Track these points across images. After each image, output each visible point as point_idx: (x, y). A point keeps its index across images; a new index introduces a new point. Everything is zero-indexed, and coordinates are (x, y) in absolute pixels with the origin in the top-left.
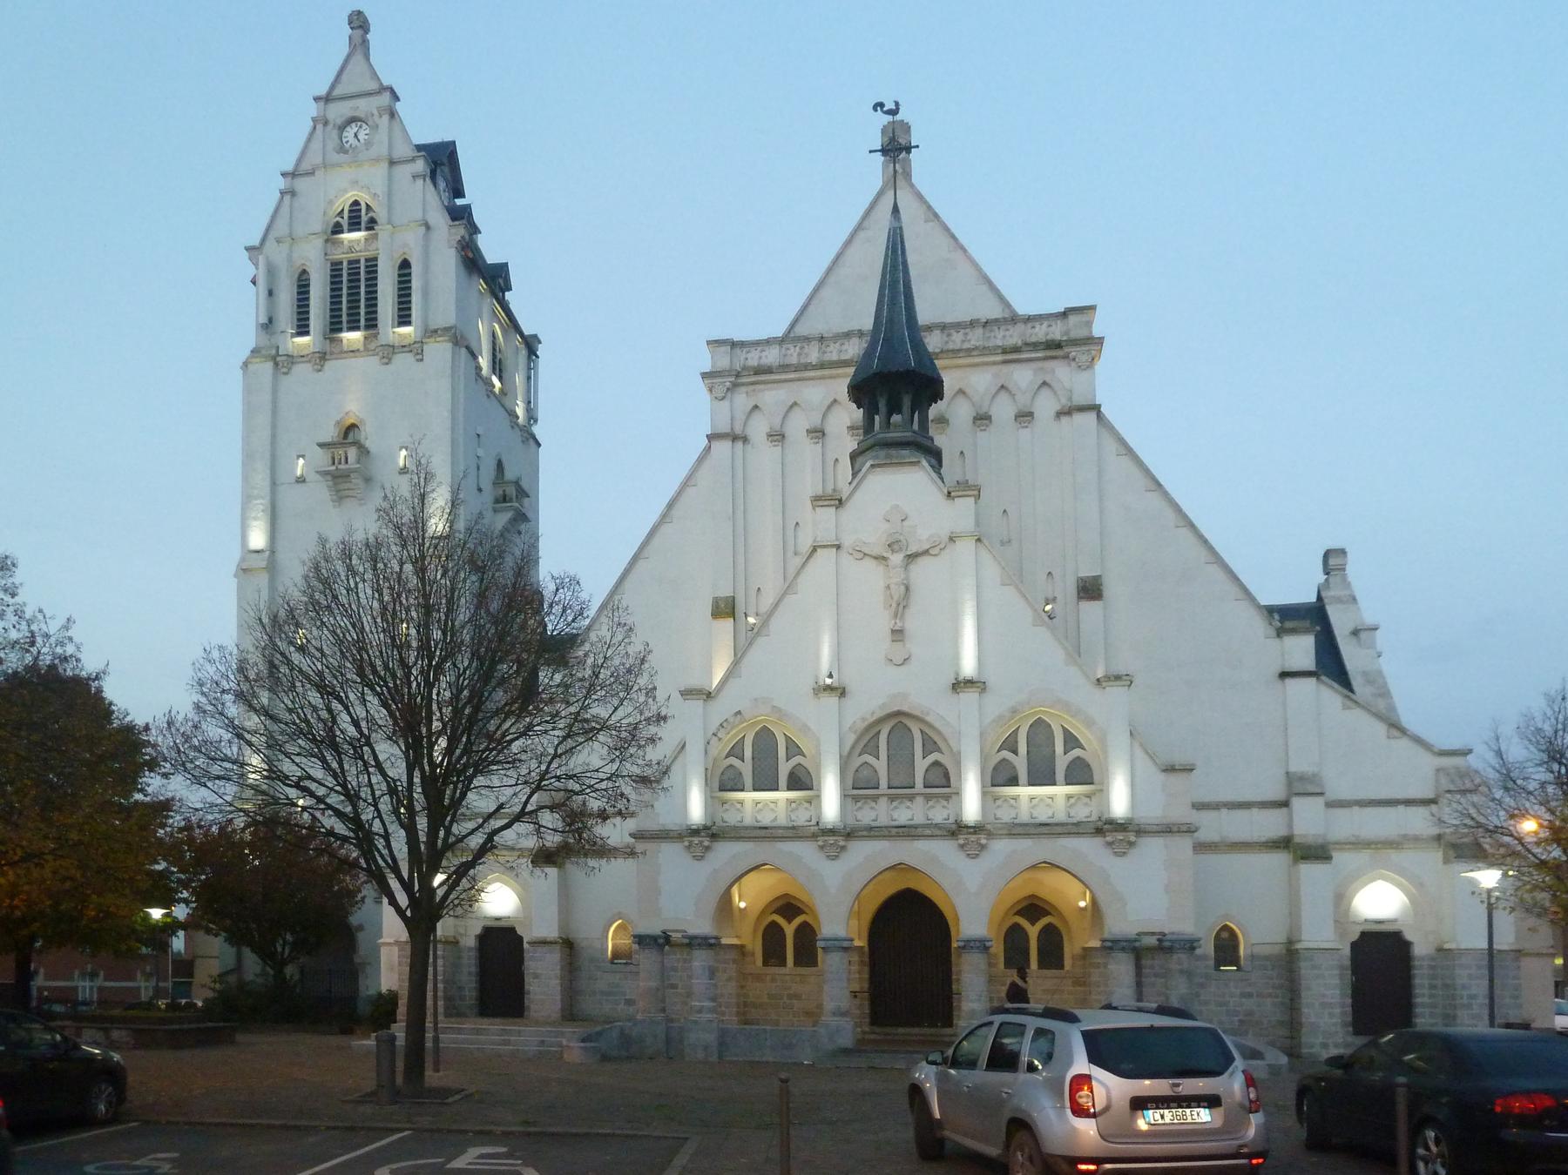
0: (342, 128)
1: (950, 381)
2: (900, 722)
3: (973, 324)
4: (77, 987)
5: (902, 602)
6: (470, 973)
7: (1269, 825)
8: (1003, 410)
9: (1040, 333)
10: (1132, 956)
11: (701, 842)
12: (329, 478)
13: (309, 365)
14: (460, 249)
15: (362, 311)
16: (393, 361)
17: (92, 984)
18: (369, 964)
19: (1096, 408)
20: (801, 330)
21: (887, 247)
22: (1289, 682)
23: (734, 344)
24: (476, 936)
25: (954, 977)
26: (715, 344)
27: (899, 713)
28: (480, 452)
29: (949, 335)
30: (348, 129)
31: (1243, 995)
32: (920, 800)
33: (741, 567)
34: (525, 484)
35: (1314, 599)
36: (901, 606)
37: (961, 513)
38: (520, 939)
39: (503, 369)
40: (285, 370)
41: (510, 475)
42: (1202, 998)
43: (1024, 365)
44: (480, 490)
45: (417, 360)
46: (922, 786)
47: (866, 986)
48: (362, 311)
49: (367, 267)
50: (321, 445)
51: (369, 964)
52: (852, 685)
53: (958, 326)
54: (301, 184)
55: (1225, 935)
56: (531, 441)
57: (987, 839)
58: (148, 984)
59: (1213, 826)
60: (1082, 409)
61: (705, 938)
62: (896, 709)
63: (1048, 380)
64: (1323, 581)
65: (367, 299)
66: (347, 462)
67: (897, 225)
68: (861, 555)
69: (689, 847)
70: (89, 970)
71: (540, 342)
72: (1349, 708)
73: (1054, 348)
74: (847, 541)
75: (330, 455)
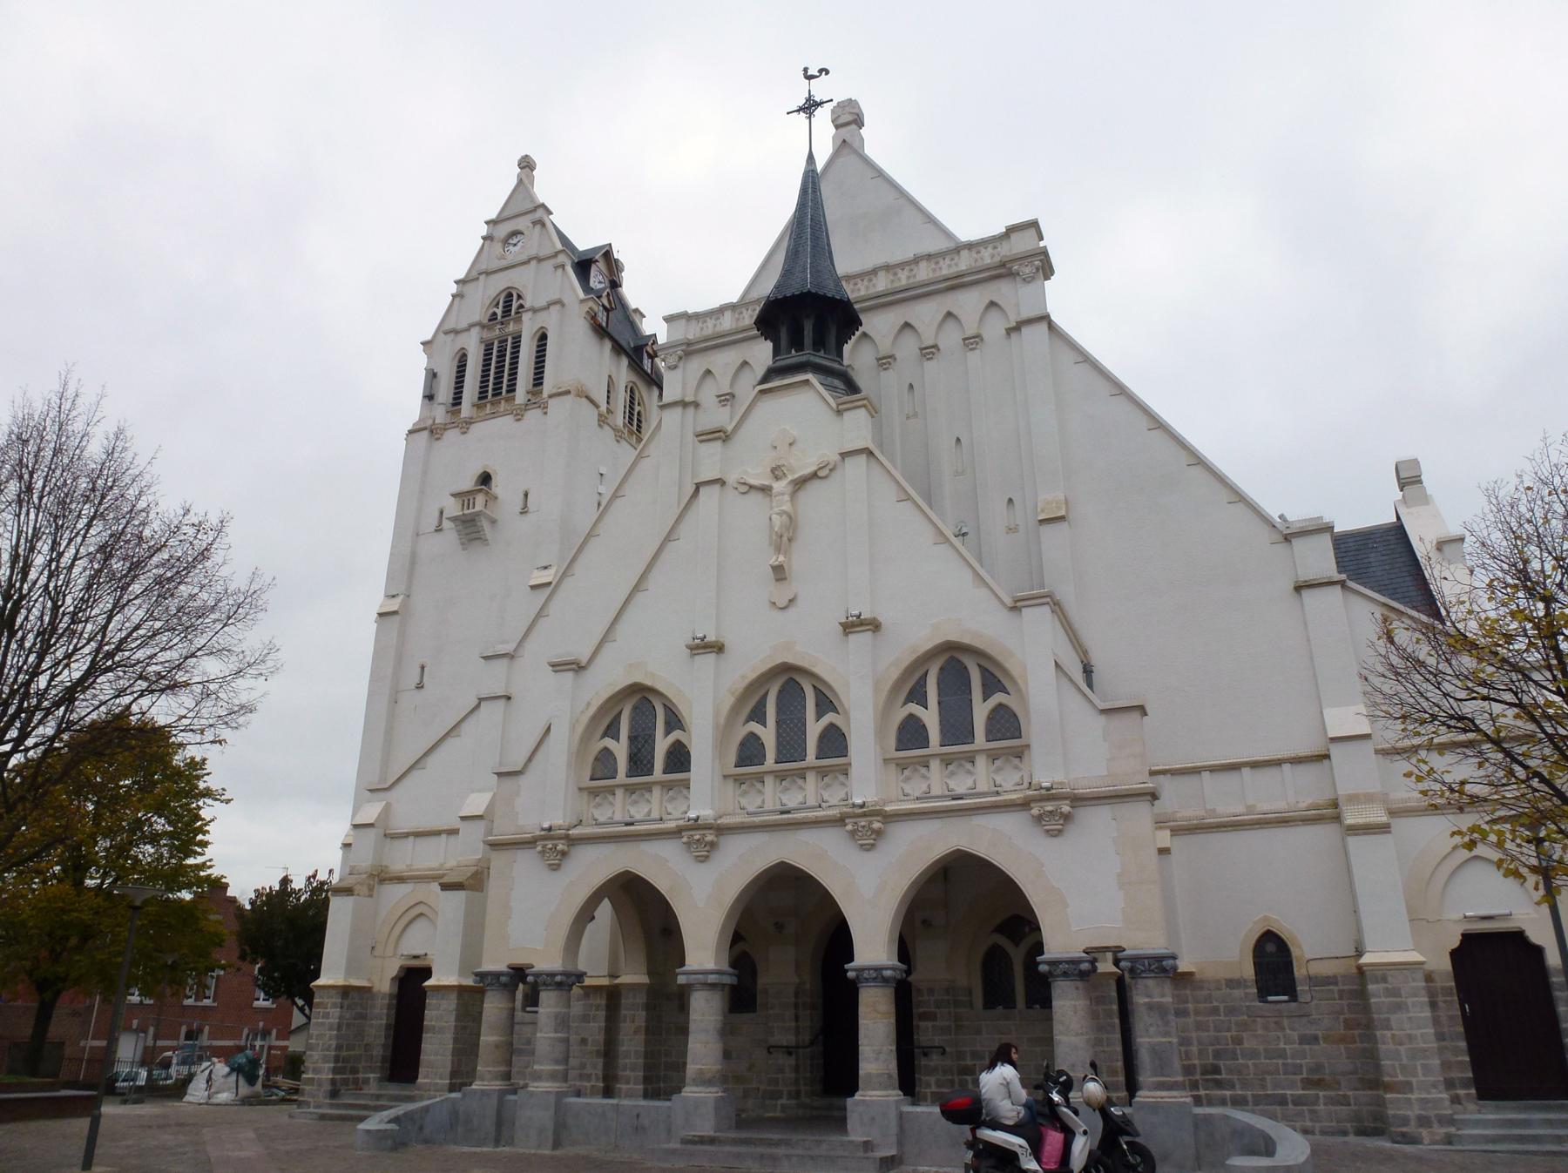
2: (791, 679)
5: (785, 538)
6: (1451, 1018)
7: (1297, 792)
8: (950, 339)
9: (987, 257)
13: (457, 429)
14: (589, 319)
15: (492, 372)
17: (263, 1043)
19: (1045, 318)
22: (1307, 595)
23: (685, 316)
24: (393, 979)
25: (392, 1033)
28: (602, 489)
31: (1304, 1040)
33: (1072, 637)
35: (1394, 519)
36: (785, 539)
37: (856, 428)
39: (643, 419)
40: (438, 436)
42: (1246, 1045)
46: (814, 757)
48: (492, 372)
52: (729, 641)
53: (902, 265)
54: (469, 288)
61: (552, 975)
63: (995, 299)
67: (811, 168)
68: (745, 489)
69: (543, 852)
73: (1004, 271)
74: (732, 479)
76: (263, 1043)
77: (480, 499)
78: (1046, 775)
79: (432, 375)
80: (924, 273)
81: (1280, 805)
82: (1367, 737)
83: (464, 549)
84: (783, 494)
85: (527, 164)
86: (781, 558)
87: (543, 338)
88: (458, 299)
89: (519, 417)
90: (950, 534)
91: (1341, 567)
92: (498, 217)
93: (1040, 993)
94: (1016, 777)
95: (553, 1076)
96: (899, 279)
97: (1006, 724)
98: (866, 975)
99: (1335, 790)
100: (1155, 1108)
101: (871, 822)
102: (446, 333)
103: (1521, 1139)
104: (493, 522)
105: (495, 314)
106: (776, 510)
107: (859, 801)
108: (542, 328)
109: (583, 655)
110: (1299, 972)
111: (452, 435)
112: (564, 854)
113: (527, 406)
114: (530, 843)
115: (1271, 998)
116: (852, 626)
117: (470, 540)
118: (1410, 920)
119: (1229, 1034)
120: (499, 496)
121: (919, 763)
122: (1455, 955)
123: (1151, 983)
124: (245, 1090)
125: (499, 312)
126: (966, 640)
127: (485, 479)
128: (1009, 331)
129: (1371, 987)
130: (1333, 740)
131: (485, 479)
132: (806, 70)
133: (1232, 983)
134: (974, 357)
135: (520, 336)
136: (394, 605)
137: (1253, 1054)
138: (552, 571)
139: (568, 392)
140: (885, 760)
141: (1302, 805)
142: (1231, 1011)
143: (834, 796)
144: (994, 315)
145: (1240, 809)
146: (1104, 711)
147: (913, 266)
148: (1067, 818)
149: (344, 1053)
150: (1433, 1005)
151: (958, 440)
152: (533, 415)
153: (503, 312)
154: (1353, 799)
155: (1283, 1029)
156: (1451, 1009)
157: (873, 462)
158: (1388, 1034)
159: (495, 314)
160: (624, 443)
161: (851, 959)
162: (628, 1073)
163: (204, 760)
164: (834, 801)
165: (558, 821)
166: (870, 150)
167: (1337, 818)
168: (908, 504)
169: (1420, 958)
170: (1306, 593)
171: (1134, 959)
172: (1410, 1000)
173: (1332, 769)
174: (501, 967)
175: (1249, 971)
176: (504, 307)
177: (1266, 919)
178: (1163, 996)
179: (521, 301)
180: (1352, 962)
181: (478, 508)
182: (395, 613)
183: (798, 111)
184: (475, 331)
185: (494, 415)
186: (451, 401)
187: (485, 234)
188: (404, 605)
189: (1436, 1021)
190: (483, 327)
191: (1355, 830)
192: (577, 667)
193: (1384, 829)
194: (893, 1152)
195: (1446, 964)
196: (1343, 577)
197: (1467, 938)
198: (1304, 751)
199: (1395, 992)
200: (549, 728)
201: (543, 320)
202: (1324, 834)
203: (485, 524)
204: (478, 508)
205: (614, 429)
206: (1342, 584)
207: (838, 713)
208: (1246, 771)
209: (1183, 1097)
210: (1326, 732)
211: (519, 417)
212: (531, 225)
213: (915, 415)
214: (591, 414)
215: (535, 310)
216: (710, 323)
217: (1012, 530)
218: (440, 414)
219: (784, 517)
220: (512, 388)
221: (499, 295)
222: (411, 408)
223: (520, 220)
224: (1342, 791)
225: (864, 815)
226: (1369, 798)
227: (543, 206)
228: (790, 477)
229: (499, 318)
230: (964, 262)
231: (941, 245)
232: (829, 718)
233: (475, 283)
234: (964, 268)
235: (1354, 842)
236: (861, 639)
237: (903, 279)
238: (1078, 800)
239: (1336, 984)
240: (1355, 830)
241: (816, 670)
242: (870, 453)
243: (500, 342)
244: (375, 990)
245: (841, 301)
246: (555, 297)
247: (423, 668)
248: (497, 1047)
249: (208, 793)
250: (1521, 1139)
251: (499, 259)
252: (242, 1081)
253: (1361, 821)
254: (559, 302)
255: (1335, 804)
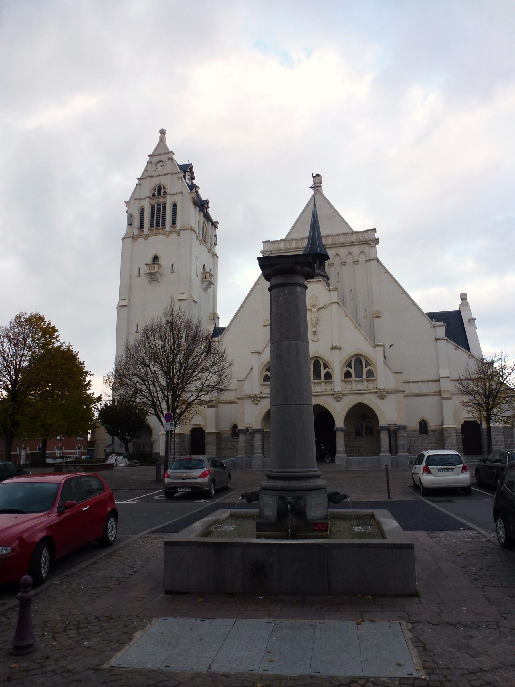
0: (156, 164)
1: (331, 253)
3: (340, 234)
4: (55, 453)
7: (432, 388)
8: (350, 260)
10: (387, 431)
11: (257, 399)
12: (149, 275)
15: (161, 220)
16: (170, 236)
17: (60, 451)
18: (157, 441)
20: (288, 238)
21: (312, 216)
26: (264, 242)
27: (316, 357)
28: (198, 263)
29: (334, 237)
30: (158, 164)
31: (429, 443)
32: (323, 383)
34: (212, 272)
35: (459, 309)
37: (334, 296)
38: (204, 431)
40: (136, 240)
41: (207, 270)
42: (416, 444)
43: (355, 246)
44: (197, 276)
45: (178, 236)
47: (445, 442)
48: (161, 220)
49: (163, 206)
50: (146, 265)
51: (157, 441)
54: (143, 182)
55: (423, 423)
56: (216, 256)
57: (343, 396)
58: (79, 451)
59: (414, 389)
60: (373, 259)
61: (259, 430)
62: (315, 355)
63: (363, 251)
64: (461, 303)
65: (162, 217)
66: (154, 270)
70: (60, 446)
71: (219, 223)
72: (456, 349)
73: (366, 242)
75: (149, 267)
76: (60, 451)
77: (156, 267)
78: (381, 386)
79: (131, 216)
80: (342, 240)
81: (428, 391)
82: (449, 377)
83: (150, 284)
84: (315, 312)
85: (163, 132)
86: (315, 329)
87: (175, 206)
88: (138, 186)
89: (168, 236)
90: (358, 326)
91: (447, 336)
92: (152, 154)
93: (379, 433)
94: (373, 386)
95: (260, 453)
96: (335, 239)
97: (370, 374)
98: (339, 429)
99: (440, 388)
100: (402, 456)
101: (340, 396)
102: (135, 200)
103: (471, 462)
104: (161, 275)
105: (154, 194)
106: (313, 316)
107: (337, 391)
108: (174, 202)
109: (261, 351)
110: (429, 429)
111: (141, 240)
112: (259, 401)
113: (170, 232)
114: (251, 398)
115: (422, 434)
116: (333, 348)
117: (152, 281)
118: (454, 418)
119: (413, 442)
120: (162, 265)
121: (350, 382)
122: (462, 425)
123: (402, 431)
124: (128, 463)
125: (156, 193)
126: (362, 354)
127: (156, 258)
128: (366, 261)
129: (445, 432)
130: (441, 377)
131: (156, 258)
132: (312, 174)
133: (414, 431)
134: (357, 267)
135: (166, 204)
136: (125, 303)
137: (417, 446)
138: (186, 294)
139: (188, 229)
140: (342, 381)
141: (433, 391)
142: (413, 437)
143: (329, 388)
144: (362, 255)
145: (418, 392)
146: (394, 373)
147: (339, 236)
148: (385, 396)
149: (181, 451)
150: (457, 436)
151: (351, 290)
152: (173, 236)
153: (158, 193)
154: (444, 391)
155: (424, 441)
156: (460, 437)
157: (338, 305)
158: (447, 442)
159: (154, 194)
160: (202, 245)
161: (335, 426)
162: (267, 453)
163: (84, 362)
164: (329, 389)
165: (258, 393)
166: (324, 193)
167: (440, 395)
168: (348, 318)
169: (455, 426)
170: (437, 341)
171: (399, 426)
172: (452, 435)
173: (440, 383)
174: (244, 428)
175: (418, 429)
176: (158, 191)
177: (422, 417)
178: (404, 434)
179: (165, 190)
180: (440, 427)
181: (156, 270)
182: (126, 306)
183: (310, 188)
184: (147, 200)
185: (158, 234)
186: (139, 226)
187: (148, 161)
188: (129, 303)
189: (457, 439)
190: (150, 198)
191: (445, 398)
192: (259, 353)
193: (451, 398)
194: (346, 466)
195: (460, 427)
196: (447, 338)
197: (465, 422)
198: (433, 379)
199: (449, 433)
200: (252, 369)
201: (174, 199)
202: (436, 398)
203: (158, 275)
204: (156, 270)
205: (208, 249)
206: (446, 340)
207: (329, 368)
208: (420, 383)
209: (407, 454)
210: (439, 375)
211: (168, 236)
212: (167, 160)
213: (339, 282)
214: (194, 236)
215: (171, 195)
216: (277, 244)
217: (366, 317)
218: (136, 232)
219: (316, 319)
220: (164, 224)
221: (156, 186)
222: (123, 228)
223: (163, 156)
224: (442, 389)
225: (339, 394)
226: (448, 391)
227: (172, 152)
228: (317, 308)
229: (156, 196)
230: (354, 238)
231: (348, 231)
232: (327, 370)
233: (145, 180)
234: (354, 240)
235: (443, 401)
236: (336, 352)
237: (336, 240)
238: (388, 392)
239: (437, 431)
240: (445, 398)
241: (325, 358)
242: (338, 303)
243: (157, 205)
244: (185, 434)
245: (327, 255)
246: (180, 191)
247: (138, 326)
248: (244, 447)
249: (87, 373)
250: (471, 462)
251: (155, 171)
252: (127, 461)
253: (446, 397)
254: (181, 193)
255: (440, 392)
